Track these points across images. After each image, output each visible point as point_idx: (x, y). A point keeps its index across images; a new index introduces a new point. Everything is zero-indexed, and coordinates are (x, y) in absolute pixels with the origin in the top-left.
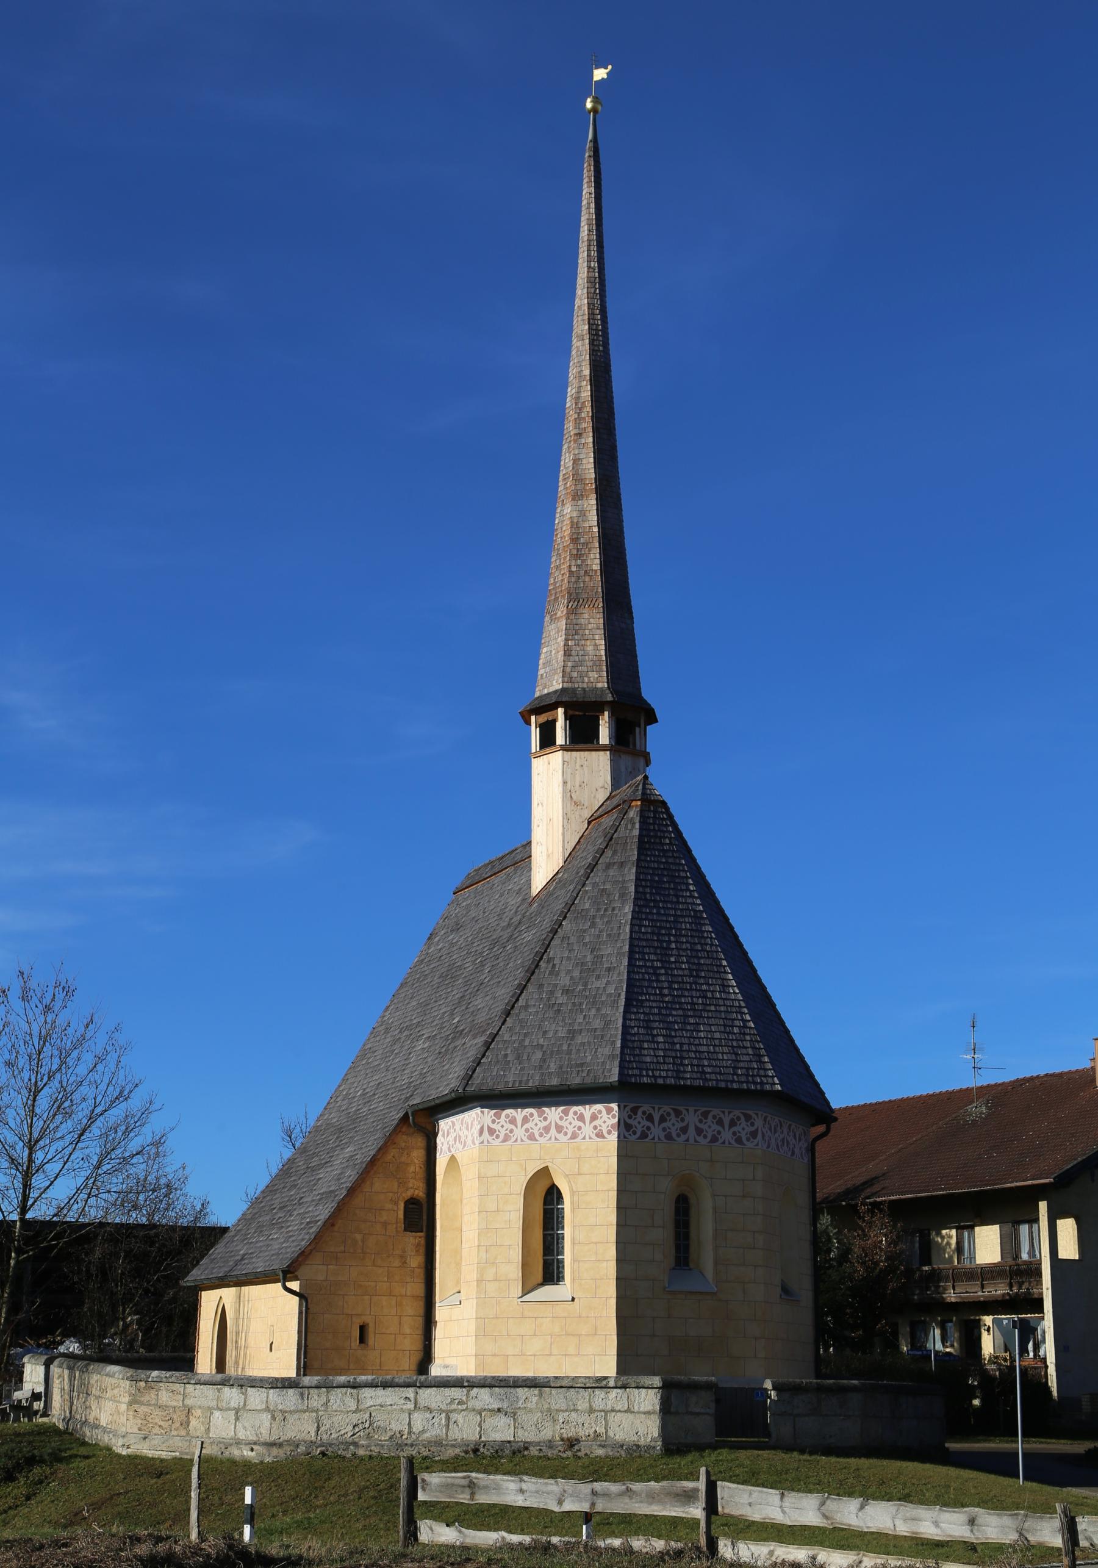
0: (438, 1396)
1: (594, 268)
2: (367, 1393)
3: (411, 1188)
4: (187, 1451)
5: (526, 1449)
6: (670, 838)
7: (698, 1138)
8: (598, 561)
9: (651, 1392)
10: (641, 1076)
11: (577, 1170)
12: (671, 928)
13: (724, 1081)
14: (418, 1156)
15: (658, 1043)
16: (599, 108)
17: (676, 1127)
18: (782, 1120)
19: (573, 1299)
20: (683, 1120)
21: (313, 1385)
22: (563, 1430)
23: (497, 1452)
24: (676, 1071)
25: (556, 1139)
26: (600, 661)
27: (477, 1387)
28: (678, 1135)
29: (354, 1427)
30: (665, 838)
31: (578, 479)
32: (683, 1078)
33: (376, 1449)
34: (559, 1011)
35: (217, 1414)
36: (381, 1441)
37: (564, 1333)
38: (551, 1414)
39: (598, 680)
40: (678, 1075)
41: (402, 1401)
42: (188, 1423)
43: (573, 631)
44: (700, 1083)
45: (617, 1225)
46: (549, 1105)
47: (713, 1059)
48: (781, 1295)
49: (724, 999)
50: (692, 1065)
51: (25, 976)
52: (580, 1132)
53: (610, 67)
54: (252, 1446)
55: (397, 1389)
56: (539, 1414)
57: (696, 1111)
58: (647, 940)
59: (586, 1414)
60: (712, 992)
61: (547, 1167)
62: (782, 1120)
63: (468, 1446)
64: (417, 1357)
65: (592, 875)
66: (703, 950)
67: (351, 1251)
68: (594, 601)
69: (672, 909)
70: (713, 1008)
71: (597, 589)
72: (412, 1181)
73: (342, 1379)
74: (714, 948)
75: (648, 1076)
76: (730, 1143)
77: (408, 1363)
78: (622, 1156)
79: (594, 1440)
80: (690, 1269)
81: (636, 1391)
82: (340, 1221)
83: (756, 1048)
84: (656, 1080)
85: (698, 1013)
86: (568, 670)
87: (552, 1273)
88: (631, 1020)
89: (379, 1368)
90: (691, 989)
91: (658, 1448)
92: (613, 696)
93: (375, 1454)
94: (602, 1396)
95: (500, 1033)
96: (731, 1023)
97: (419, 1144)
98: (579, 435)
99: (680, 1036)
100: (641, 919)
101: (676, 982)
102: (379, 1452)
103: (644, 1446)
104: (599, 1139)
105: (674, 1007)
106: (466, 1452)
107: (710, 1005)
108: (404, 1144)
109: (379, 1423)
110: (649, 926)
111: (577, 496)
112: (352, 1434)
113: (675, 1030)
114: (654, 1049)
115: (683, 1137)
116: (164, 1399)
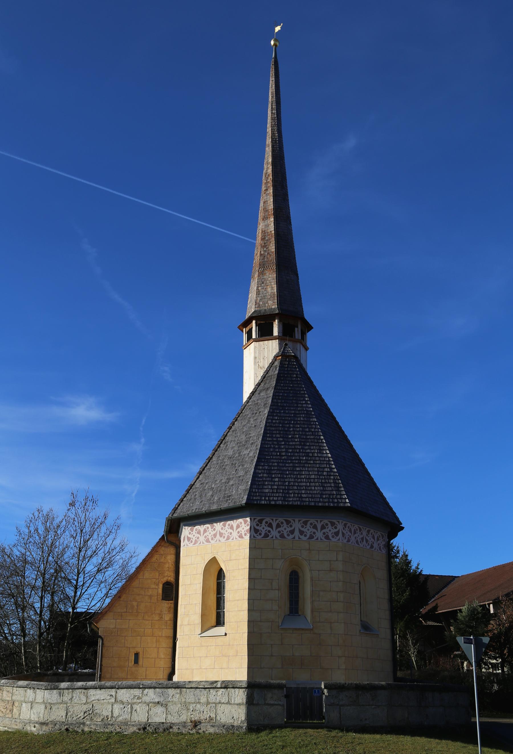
0: (127, 694)
1: (274, 113)
2: (92, 692)
3: (167, 576)
4: (10, 727)
5: (171, 727)
6: (297, 374)
7: (301, 537)
8: (274, 247)
9: (242, 691)
10: (261, 500)
11: (229, 558)
12: (291, 420)
13: (313, 501)
14: (171, 558)
15: (274, 482)
16: (278, 44)
17: (286, 530)
18: (361, 527)
19: (226, 634)
20: (291, 526)
21: (65, 688)
22: (192, 716)
23: (155, 729)
24: (283, 497)
25: (219, 541)
26: (274, 295)
27: (147, 688)
28: (288, 535)
29: (84, 713)
30: (293, 374)
31: (266, 210)
32: (288, 501)
33: (93, 727)
34: (225, 468)
35: (24, 705)
36: (97, 722)
37: (221, 655)
38: (186, 705)
39: (272, 305)
40: (285, 499)
41: (109, 697)
42: (13, 710)
43: (262, 283)
44: (298, 503)
45: (249, 589)
46: (217, 521)
47: (308, 490)
48: (360, 630)
49: (319, 457)
50: (294, 493)
51: (74, 495)
52: (231, 536)
53: (282, 24)
54: (35, 724)
55: (107, 690)
56: (180, 705)
57: (299, 521)
58: (275, 427)
59: (205, 705)
60: (313, 453)
61: (215, 557)
62: (361, 527)
63: (141, 725)
64: (168, 671)
65: (253, 396)
66: (310, 431)
67: (130, 611)
68: (272, 266)
69: (293, 410)
70: (312, 462)
71: (273, 260)
72: (167, 572)
73: (80, 684)
74: (316, 430)
75: (265, 500)
76: (321, 539)
77: (162, 676)
78: (252, 548)
79: (209, 722)
80: (299, 615)
81: (233, 690)
82: (124, 595)
83: (337, 483)
84: (270, 502)
85: (302, 465)
86: (258, 301)
87: (220, 621)
88: (259, 469)
89: (145, 678)
90: (300, 452)
91: (244, 728)
92: (279, 311)
93: (93, 730)
94: (214, 693)
95: (195, 484)
96: (322, 470)
97: (172, 552)
98: (267, 190)
99: (289, 478)
100: (273, 416)
101: (291, 449)
102: (95, 729)
103: (236, 726)
104: (240, 539)
105: (288, 462)
106: (139, 729)
107: (310, 460)
108: (163, 552)
109: (97, 711)
110: (278, 419)
111: (265, 218)
112: (83, 717)
113: (287, 474)
114: (272, 485)
115: (291, 536)
116: (5, 696)
